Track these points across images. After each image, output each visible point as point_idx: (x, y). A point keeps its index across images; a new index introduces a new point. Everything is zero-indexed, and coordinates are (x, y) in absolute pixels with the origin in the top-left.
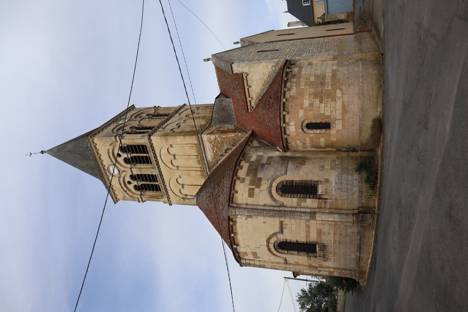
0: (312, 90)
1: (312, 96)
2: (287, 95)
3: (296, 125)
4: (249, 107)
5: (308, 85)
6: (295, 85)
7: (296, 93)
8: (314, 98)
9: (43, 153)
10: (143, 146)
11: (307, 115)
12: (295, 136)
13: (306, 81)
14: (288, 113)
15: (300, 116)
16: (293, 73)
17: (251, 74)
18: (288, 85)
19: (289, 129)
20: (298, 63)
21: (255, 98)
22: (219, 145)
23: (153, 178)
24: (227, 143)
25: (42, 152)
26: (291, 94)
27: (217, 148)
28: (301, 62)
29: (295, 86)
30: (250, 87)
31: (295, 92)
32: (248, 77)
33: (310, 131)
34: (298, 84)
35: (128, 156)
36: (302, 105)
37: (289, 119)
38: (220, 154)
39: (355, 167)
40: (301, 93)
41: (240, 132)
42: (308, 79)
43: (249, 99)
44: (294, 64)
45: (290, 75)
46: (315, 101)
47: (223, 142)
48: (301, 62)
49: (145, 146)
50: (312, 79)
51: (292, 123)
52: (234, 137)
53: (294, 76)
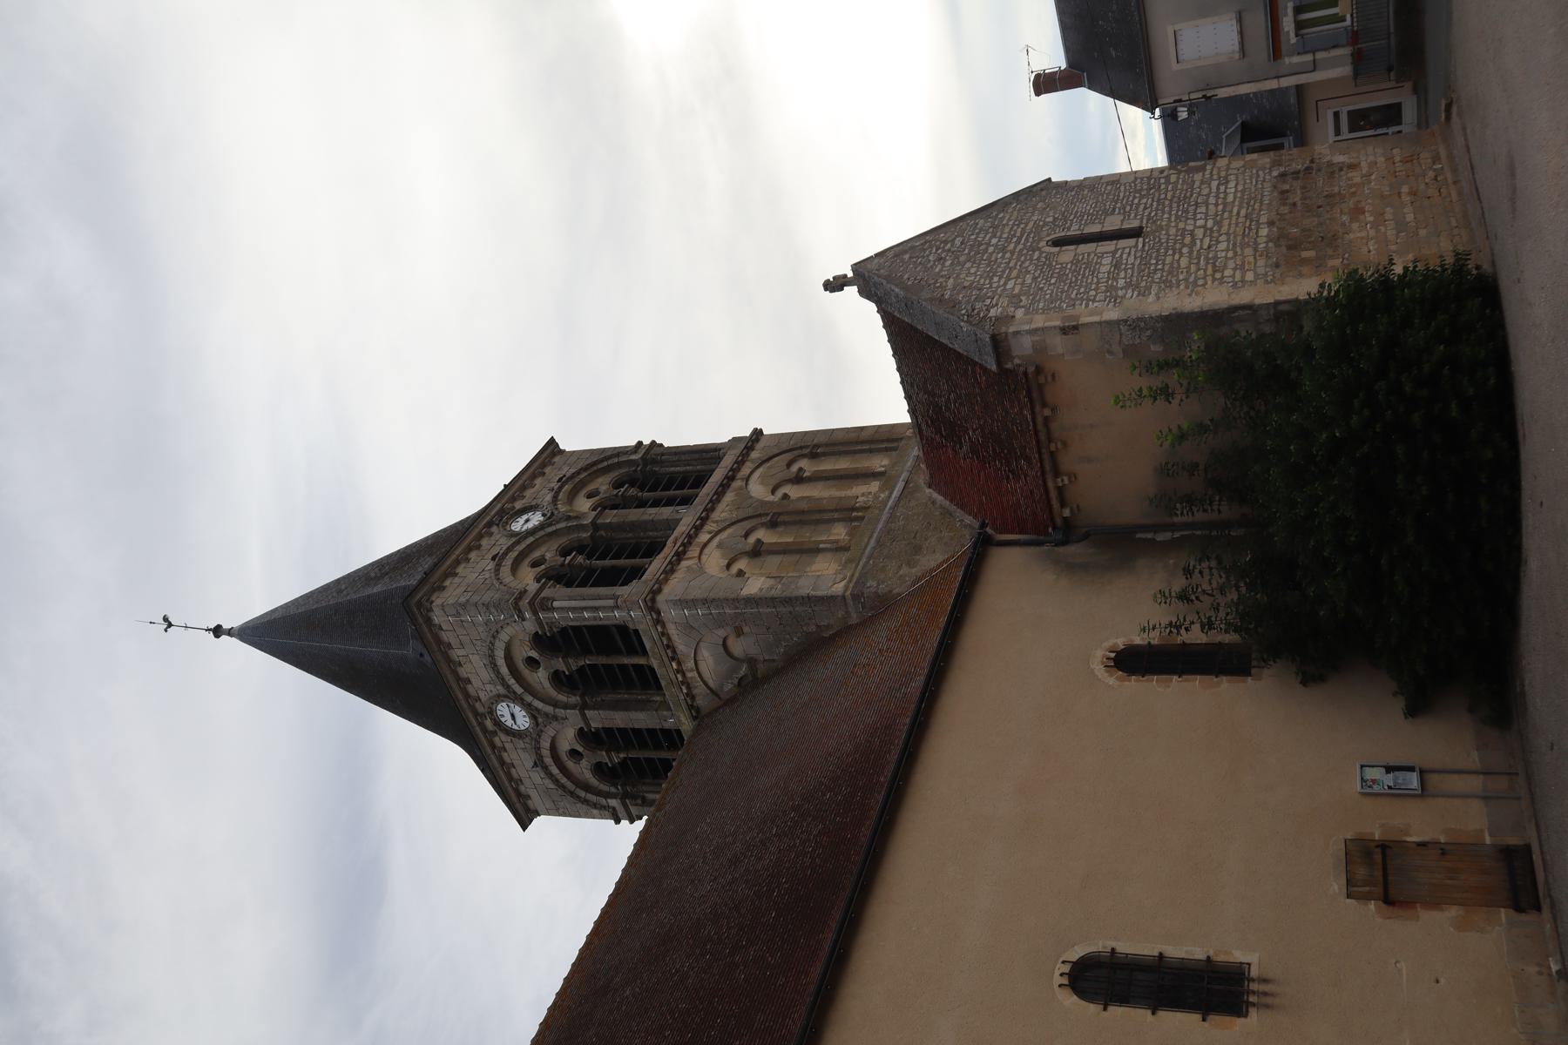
9: (217, 636)
10: (623, 629)
23: (627, 639)
25: (218, 631)
35: (567, 664)
39: (1400, 704)
49: (636, 631)
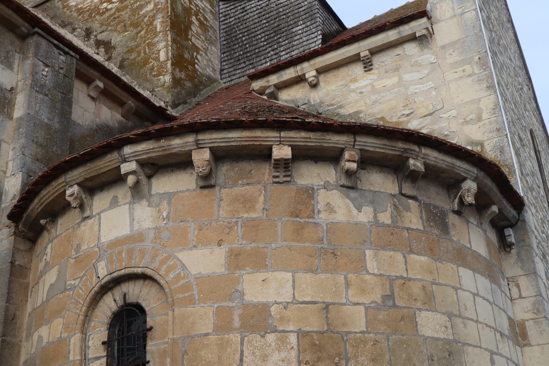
0: (357, 320)
1: (314, 324)
2: (311, 175)
3: (137, 237)
4: (274, 79)
5: (390, 297)
6: (385, 218)
7: (333, 227)
8: (301, 334)
11: (191, 301)
12: (79, 246)
13: (416, 288)
14: (207, 182)
15: (185, 257)
16: (452, 219)
17: (427, 56)
18: (380, 182)
19: (114, 203)
20: (511, 266)
21: (315, 96)
22: (125, 15)
24: (134, 39)
26: (323, 198)
27: (118, 10)
28: (523, 282)
29: (376, 223)
30: (368, 66)
31: (341, 216)
32: (411, 48)
33: (99, 333)
34: (389, 238)
36: (259, 261)
37: (169, 196)
38: (96, 25)
40: (331, 252)
41: (176, 82)
42: (430, 302)
43: (309, 69)
44: (505, 246)
45: (440, 200)
46: (283, 341)
47: (136, 25)
48: (523, 282)
50: (430, 324)
51: (145, 216)
52: (157, 59)
53: (437, 219)
